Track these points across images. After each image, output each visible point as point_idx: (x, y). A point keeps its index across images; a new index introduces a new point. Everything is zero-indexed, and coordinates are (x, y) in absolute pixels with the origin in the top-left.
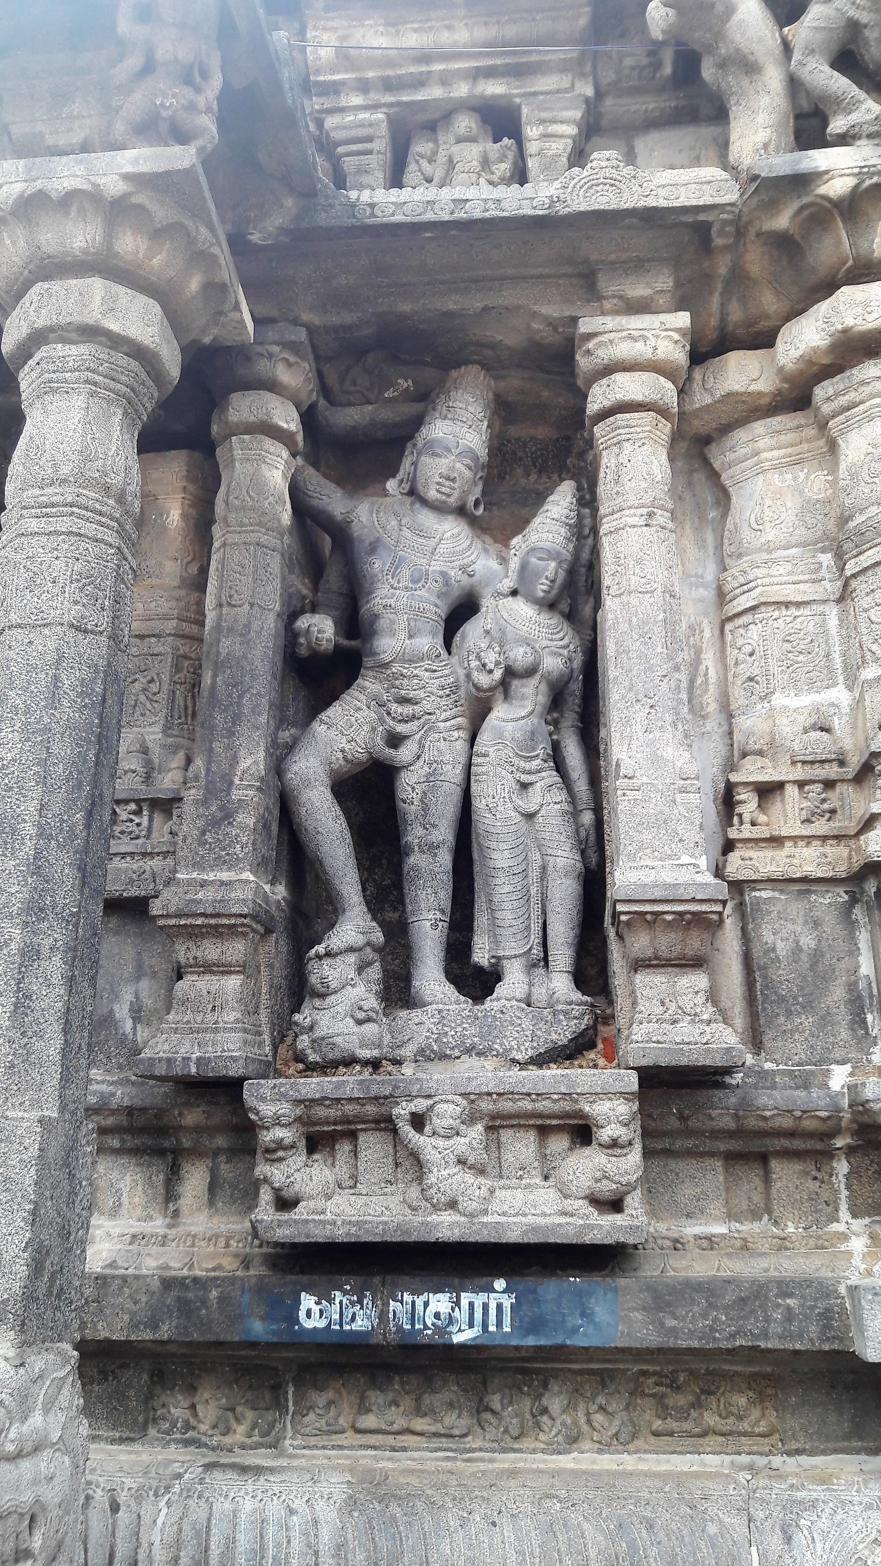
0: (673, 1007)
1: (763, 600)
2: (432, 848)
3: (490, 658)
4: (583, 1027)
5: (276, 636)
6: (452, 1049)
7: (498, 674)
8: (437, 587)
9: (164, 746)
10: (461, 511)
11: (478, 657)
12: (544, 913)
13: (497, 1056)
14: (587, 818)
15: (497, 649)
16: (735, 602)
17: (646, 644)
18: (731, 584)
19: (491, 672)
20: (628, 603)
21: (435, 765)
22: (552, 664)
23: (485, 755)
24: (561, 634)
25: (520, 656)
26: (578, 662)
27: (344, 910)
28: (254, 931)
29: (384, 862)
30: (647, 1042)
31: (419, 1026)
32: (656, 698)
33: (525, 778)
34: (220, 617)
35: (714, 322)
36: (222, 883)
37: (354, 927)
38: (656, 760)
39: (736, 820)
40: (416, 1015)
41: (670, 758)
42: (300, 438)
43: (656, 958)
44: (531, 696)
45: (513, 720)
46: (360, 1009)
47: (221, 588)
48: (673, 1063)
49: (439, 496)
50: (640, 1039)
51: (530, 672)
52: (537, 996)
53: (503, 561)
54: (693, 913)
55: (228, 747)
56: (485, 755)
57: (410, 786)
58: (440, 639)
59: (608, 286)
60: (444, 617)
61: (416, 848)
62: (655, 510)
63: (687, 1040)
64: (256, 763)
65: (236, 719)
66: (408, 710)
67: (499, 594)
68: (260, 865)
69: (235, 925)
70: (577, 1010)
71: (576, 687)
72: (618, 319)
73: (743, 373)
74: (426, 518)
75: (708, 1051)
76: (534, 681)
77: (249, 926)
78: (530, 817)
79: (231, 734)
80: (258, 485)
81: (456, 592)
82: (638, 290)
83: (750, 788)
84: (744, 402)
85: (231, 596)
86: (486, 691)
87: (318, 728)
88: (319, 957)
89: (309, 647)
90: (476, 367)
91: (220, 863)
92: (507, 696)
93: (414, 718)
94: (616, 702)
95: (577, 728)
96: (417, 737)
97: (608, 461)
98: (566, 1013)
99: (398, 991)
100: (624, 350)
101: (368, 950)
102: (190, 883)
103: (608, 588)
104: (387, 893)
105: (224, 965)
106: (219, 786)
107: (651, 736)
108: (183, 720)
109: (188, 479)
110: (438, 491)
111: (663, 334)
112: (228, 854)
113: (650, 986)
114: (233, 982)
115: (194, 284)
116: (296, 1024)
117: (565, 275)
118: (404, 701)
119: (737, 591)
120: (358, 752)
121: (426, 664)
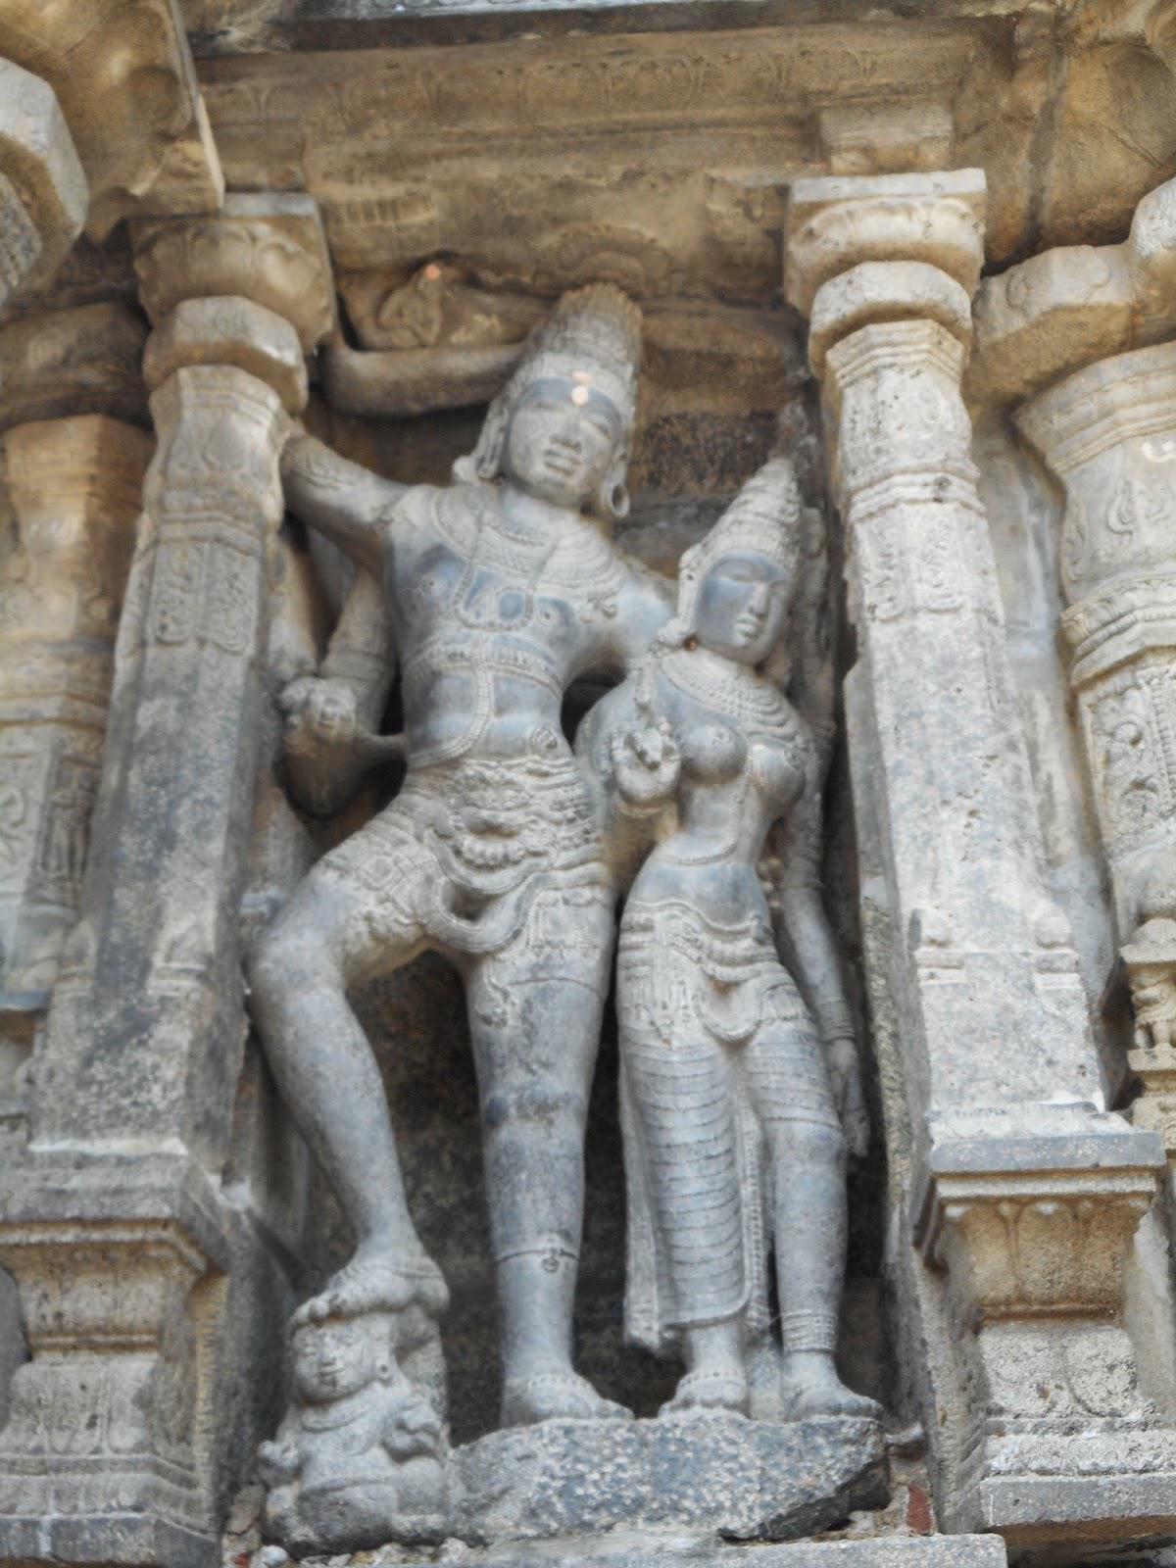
0: (1064, 1399)
1: (1150, 642)
2: (543, 1109)
3: (653, 743)
4: (865, 1460)
5: (245, 702)
6: (596, 1509)
7: (669, 772)
8: (551, 624)
9: (26, 920)
10: (587, 509)
11: (630, 742)
12: (771, 1238)
13: (688, 1523)
14: (845, 1053)
15: (665, 727)
16: (1095, 655)
17: (952, 700)
18: (1083, 623)
19: (654, 767)
20: (912, 630)
21: (547, 950)
22: (766, 758)
23: (647, 928)
24: (779, 717)
25: (709, 742)
26: (812, 767)
27: (368, 1232)
28: (182, 1259)
29: (446, 1158)
30: (1020, 1471)
31: (525, 1459)
32: (980, 797)
33: (725, 973)
34: (139, 669)
35: (1022, 202)
36: (121, 1161)
37: (389, 1263)
38: (987, 910)
39: (1140, 1037)
40: (517, 1439)
41: (1016, 906)
42: (302, 381)
43: (1023, 1299)
44: (728, 826)
45: (696, 862)
46: (402, 1426)
47: (145, 614)
48: (1079, 1515)
49: (550, 474)
50: (1004, 1467)
51: (732, 768)
52: (760, 1410)
53: (670, 596)
54: (1095, 1198)
55: (146, 898)
56: (647, 928)
57: (500, 994)
58: (554, 721)
59: (845, 132)
60: (560, 678)
61: (513, 1111)
62: (950, 477)
63: (1103, 1465)
64: (198, 927)
65: (167, 841)
66: (494, 848)
67: (659, 646)
68: (204, 1127)
69: (143, 1243)
70: (851, 1426)
71: (810, 812)
72: (860, 181)
73: (1076, 281)
74: (527, 512)
75: (1150, 1485)
76: (736, 791)
77: (173, 1247)
78: (736, 1047)
79: (152, 871)
80: (220, 442)
81: (582, 641)
82: (889, 134)
83: (1163, 975)
84: (1081, 325)
85: (163, 628)
86: (646, 804)
87: (325, 877)
88: (316, 1321)
89: (308, 730)
90: (612, 289)
91: (117, 1120)
92: (684, 817)
93: (506, 861)
94: (903, 808)
95: (817, 889)
96: (512, 898)
97: (855, 406)
98: (829, 1431)
99: (477, 1402)
100: (872, 228)
101: (417, 1313)
102: (55, 1160)
103: (873, 608)
104: (459, 1212)
105: (118, 1331)
106: (123, 966)
107: (976, 866)
108: (65, 871)
109: (98, 461)
110: (549, 465)
111: (941, 207)
112: (135, 1104)
113: (1013, 1359)
114: (135, 1369)
115: (117, 64)
116: (267, 1463)
117: (764, 122)
118: (489, 830)
119: (1099, 635)
120: (398, 922)
121: (530, 760)
